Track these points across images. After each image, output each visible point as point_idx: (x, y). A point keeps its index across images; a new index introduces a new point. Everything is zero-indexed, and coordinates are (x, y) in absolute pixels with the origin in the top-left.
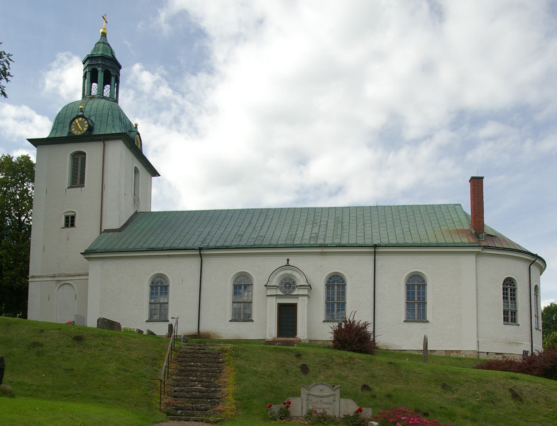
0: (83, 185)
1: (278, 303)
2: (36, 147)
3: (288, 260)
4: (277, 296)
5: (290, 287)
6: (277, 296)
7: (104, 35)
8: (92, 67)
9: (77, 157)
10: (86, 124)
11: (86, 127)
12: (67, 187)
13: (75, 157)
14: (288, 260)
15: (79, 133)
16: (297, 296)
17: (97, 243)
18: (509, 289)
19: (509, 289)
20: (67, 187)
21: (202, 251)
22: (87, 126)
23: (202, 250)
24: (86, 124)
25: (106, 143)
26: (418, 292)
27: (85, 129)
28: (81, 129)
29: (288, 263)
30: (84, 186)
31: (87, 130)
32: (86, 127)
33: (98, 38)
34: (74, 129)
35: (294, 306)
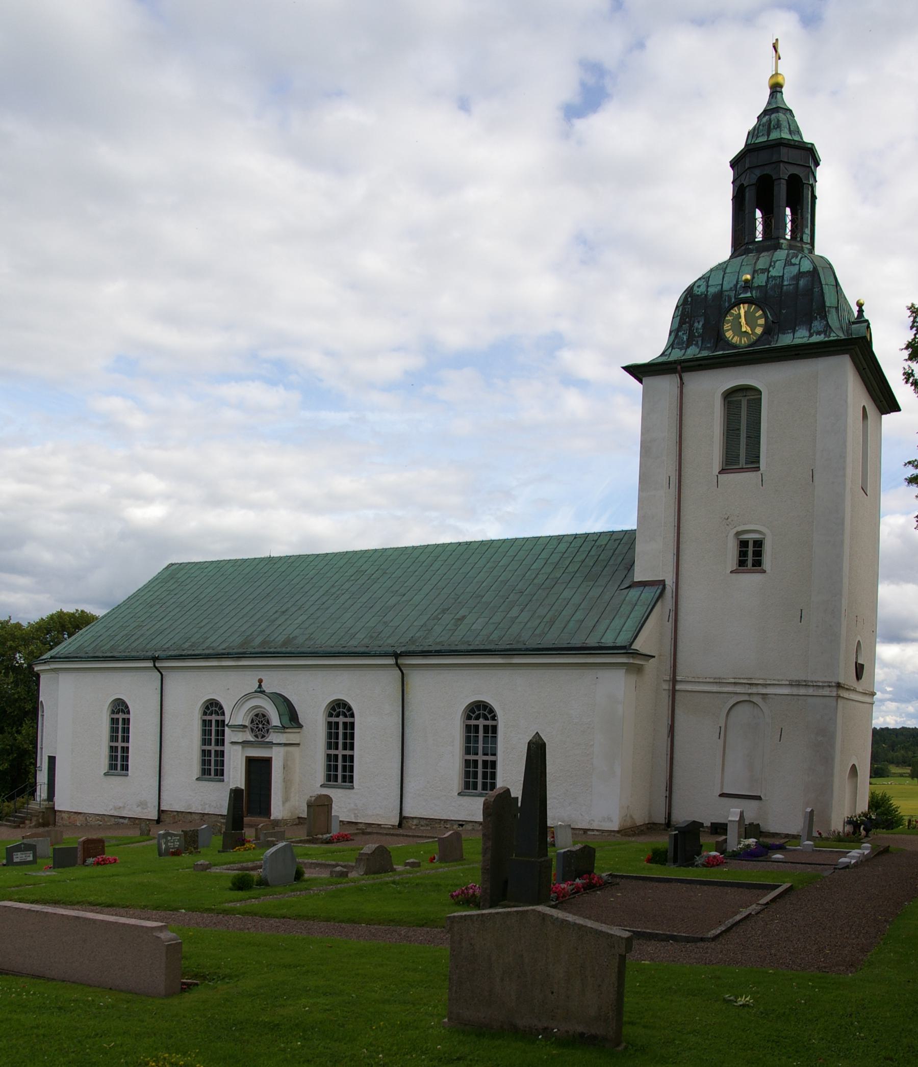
0: (757, 466)
1: (246, 757)
2: (641, 382)
3: (260, 681)
4: (245, 744)
5: (257, 728)
6: (245, 744)
7: (776, 89)
8: (758, 173)
9: (739, 398)
10: (760, 317)
11: (760, 325)
12: (718, 471)
13: (729, 399)
14: (260, 681)
15: (744, 341)
16: (271, 744)
17: (264, 630)
18: (480, 751)
19: (480, 751)
20: (716, 468)
21: (158, 662)
22: (762, 321)
23: (157, 661)
24: (760, 317)
25: (687, 376)
26: (483, 747)
27: (759, 331)
28: (750, 332)
29: (260, 686)
30: (759, 467)
31: (764, 333)
32: (760, 325)
33: (761, 101)
34: (731, 332)
35: (268, 761)
